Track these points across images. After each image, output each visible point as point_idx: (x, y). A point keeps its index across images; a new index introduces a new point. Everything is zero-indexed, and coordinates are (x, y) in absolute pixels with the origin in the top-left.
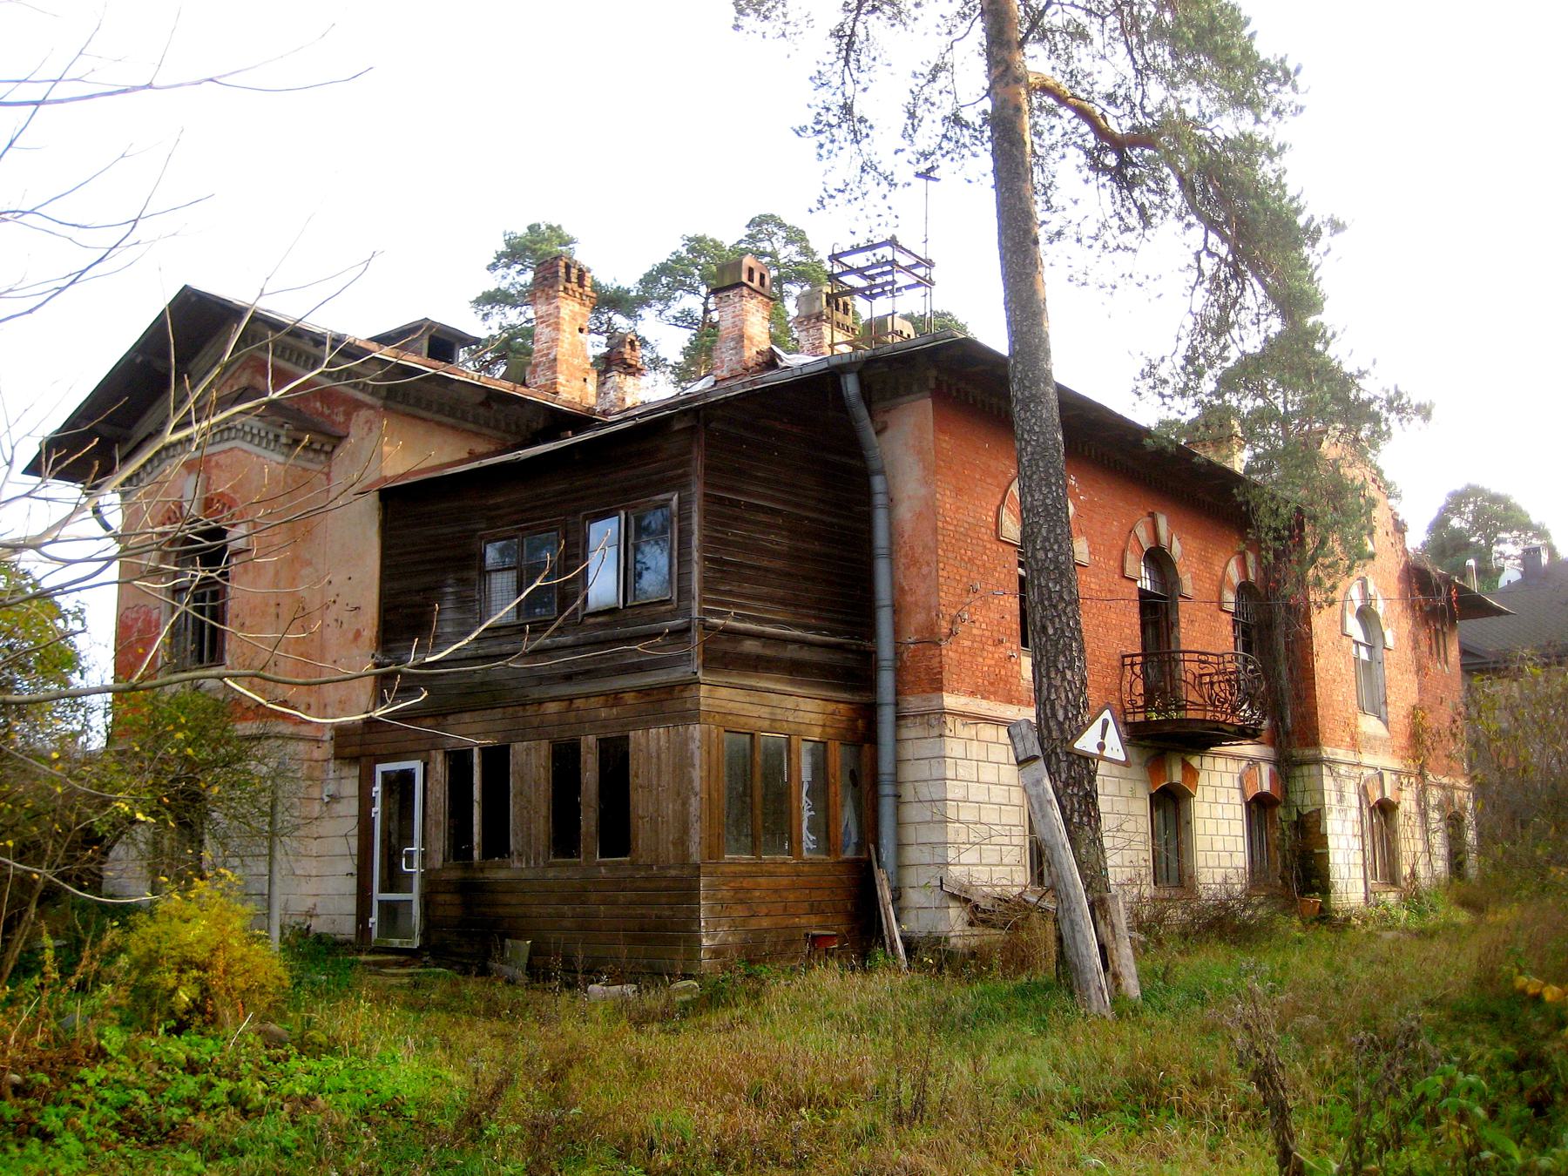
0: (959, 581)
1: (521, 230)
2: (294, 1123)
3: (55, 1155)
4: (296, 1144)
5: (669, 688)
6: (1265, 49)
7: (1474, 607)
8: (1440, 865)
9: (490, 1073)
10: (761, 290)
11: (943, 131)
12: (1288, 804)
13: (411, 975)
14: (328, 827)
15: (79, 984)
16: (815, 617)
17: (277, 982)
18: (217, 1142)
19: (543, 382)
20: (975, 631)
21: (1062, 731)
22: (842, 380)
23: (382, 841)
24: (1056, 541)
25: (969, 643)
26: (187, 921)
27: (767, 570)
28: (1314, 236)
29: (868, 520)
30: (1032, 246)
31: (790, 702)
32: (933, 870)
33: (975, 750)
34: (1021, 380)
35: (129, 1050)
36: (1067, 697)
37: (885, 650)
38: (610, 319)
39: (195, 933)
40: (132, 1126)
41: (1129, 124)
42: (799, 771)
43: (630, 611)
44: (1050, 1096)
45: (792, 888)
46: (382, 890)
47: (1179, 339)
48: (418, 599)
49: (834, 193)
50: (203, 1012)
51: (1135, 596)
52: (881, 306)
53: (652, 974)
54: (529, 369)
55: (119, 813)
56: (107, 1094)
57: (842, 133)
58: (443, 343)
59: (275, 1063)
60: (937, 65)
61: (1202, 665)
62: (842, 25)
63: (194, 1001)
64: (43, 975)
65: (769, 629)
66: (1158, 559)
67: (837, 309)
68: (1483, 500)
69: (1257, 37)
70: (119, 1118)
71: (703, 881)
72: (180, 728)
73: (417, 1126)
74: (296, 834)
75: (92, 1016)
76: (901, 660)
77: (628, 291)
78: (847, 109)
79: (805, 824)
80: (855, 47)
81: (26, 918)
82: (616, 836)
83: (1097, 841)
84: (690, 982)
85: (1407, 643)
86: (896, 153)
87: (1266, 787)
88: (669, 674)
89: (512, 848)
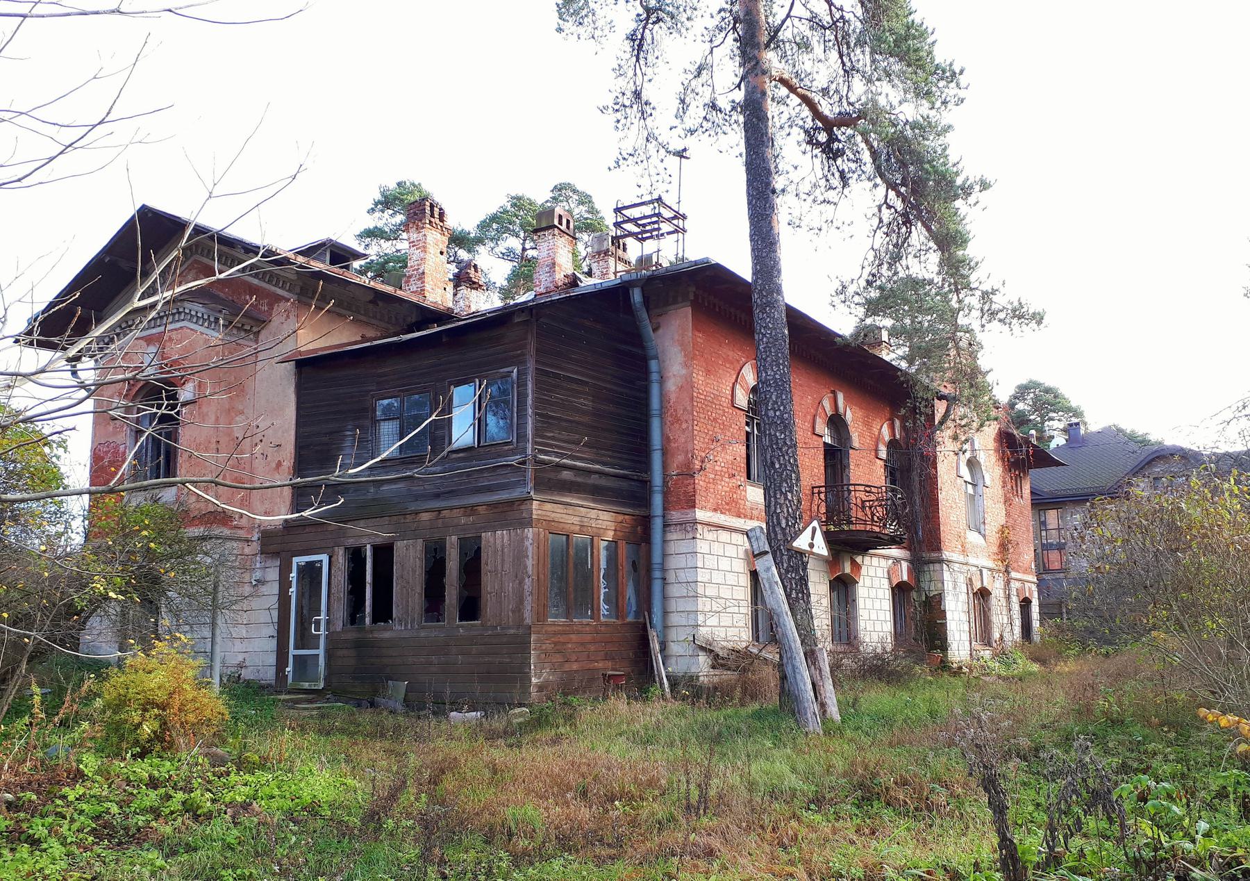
0: (707, 434)
1: (392, 185)
2: (235, 824)
3: (41, 857)
4: (237, 841)
5: (510, 503)
6: (941, 56)
7: (1042, 459)
8: (1017, 630)
9: (385, 780)
10: (567, 231)
11: (704, 114)
12: (919, 590)
13: (319, 708)
14: (255, 603)
15: (61, 721)
16: (610, 457)
17: (220, 716)
18: (176, 841)
19: (415, 289)
20: (717, 468)
21: (784, 534)
22: (631, 292)
23: (297, 613)
24: (782, 403)
25: (713, 476)
26: (150, 672)
27: (578, 423)
28: (967, 191)
29: (646, 391)
30: (771, 195)
31: (593, 514)
32: (689, 631)
33: (717, 549)
34: (761, 291)
35: (103, 772)
36: (788, 510)
37: (657, 479)
38: (456, 252)
39: (157, 681)
40: (104, 830)
41: (837, 111)
42: (599, 561)
43: (481, 450)
44: (793, 792)
45: (593, 642)
46: (296, 648)
47: (863, 268)
48: (325, 439)
49: (626, 157)
50: (162, 740)
51: (822, 445)
52: (650, 246)
53: (493, 704)
54: (404, 280)
55: (95, 592)
56: (85, 806)
57: (634, 112)
58: (340, 255)
59: (219, 778)
60: (701, 64)
61: (867, 494)
62: (635, 31)
63: (155, 732)
64: (32, 715)
65: (578, 464)
66: (837, 422)
67: (619, 248)
68: (1040, 391)
69: (936, 44)
70: (94, 826)
71: (533, 637)
72: (146, 527)
73: (331, 823)
74: (234, 607)
75: (73, 746)
76: (667, 487)
77: (469, 233)
78: (637, 95)
79: (602, 598)
80: (644, 48)
81: (18, 672)
82: (470, 609)
83: (808, 610)
84: (524, 709)
85: (999, 483)
86: (671, 129)
87: (905, 578)
88: (510, 493)
89: (394, 616)
